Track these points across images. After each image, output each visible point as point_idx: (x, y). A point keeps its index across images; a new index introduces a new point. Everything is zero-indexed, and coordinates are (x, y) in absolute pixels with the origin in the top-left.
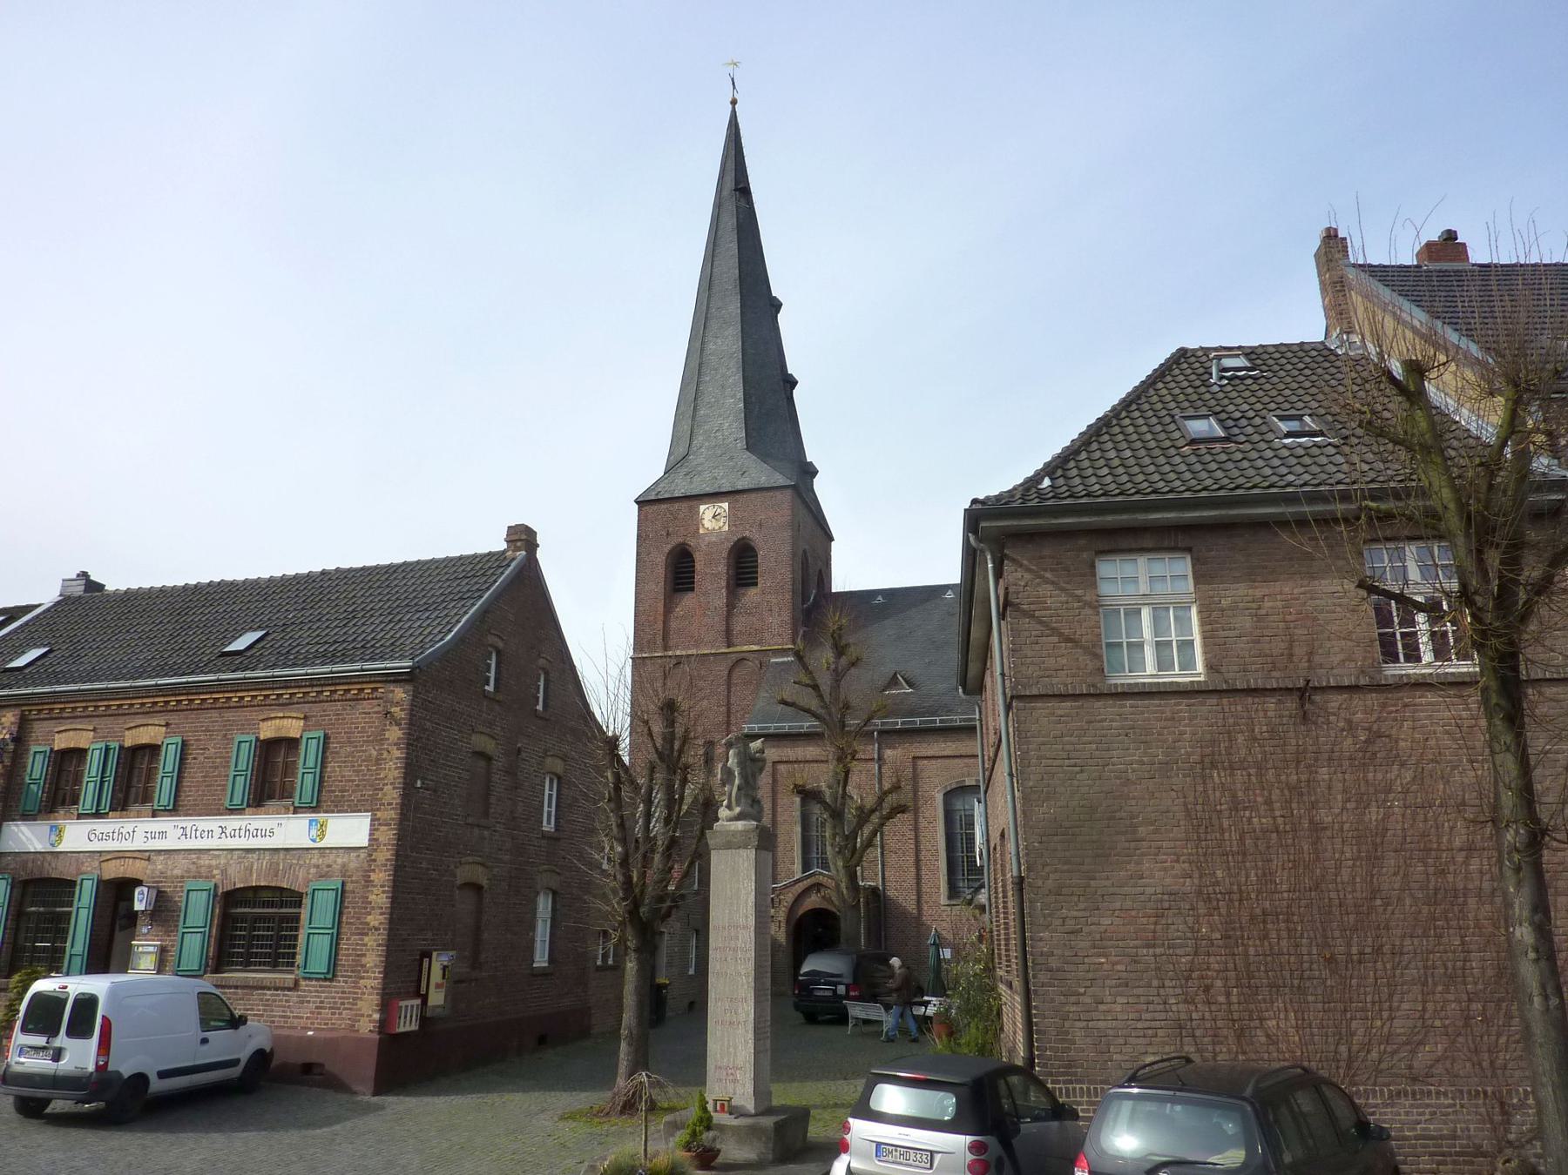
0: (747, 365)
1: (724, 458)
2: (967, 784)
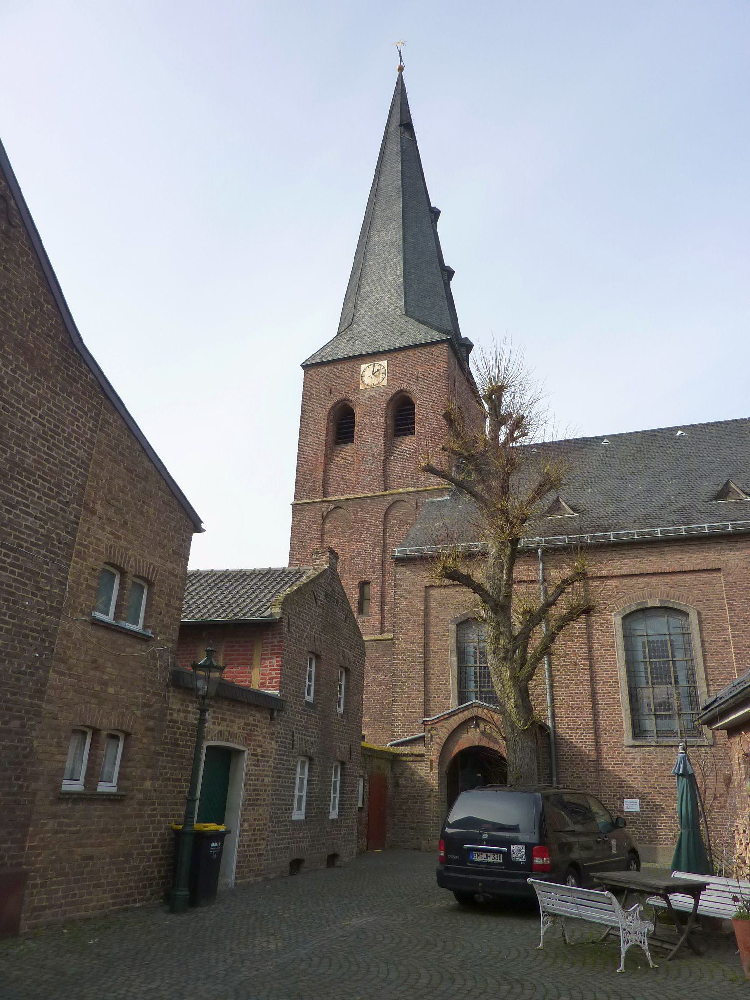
0: (403, 152)
2: (650, 606)
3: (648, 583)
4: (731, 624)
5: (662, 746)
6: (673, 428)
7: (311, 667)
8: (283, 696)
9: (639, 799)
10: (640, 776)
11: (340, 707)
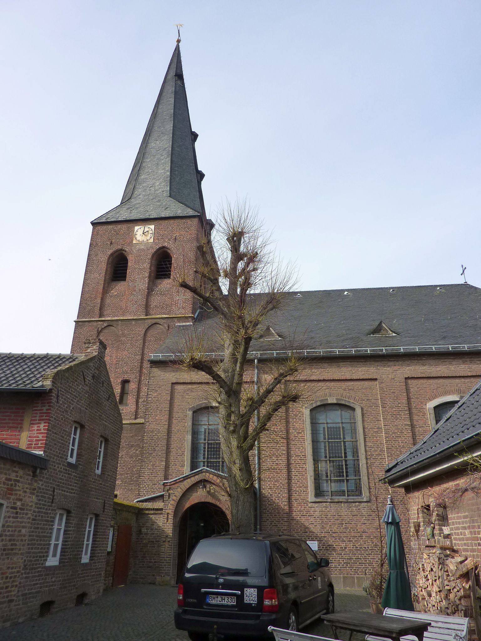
0: (176, 93)
1: (154, 200)
2: (329, 402)
3: (329, 386)
4: (383, 416)
5: (335, 502)
6: (342, 290)
7: (75, 434)
8: (47, 456)
9: (318, 541)
10: (319, 524)
11: (98, 469)
